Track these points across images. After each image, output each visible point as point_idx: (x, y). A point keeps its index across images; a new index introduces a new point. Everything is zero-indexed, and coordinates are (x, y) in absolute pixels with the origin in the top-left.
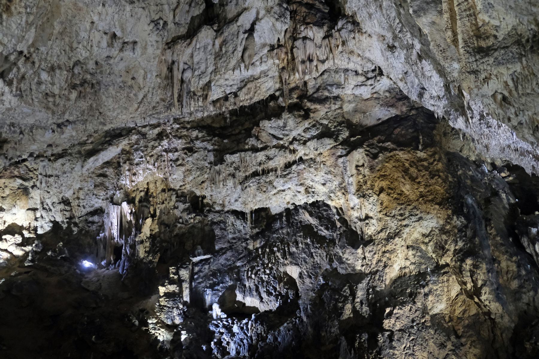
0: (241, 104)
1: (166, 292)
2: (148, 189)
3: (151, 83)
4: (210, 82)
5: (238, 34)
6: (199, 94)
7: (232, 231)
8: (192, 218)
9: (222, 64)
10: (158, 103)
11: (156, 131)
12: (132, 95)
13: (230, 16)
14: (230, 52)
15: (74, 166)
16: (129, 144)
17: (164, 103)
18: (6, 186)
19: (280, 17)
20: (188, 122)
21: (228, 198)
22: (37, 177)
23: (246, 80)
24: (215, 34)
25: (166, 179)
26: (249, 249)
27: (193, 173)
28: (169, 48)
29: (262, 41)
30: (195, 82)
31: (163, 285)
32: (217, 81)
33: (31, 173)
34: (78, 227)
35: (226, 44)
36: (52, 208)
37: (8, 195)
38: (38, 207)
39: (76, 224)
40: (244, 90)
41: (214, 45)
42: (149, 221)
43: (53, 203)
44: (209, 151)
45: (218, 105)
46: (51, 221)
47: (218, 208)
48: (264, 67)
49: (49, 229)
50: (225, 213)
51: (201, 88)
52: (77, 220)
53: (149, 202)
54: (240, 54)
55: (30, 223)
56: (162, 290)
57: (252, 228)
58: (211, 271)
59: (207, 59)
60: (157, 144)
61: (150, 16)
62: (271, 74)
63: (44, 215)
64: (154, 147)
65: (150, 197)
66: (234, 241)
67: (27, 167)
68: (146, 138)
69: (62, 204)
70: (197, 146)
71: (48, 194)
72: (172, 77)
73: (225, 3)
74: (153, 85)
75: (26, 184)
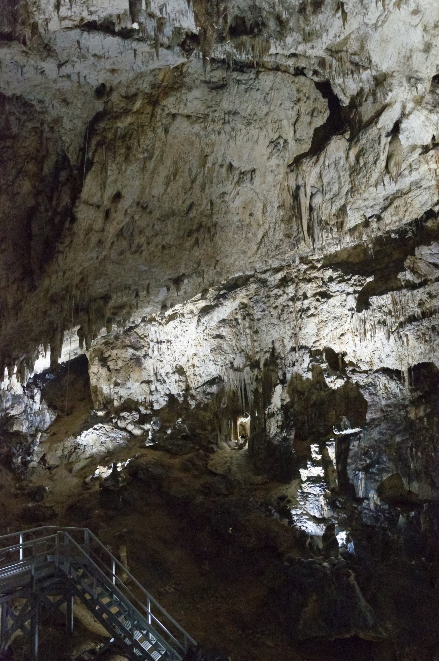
0: (388, 228)
1: (309, 476)
2: (273, 349)
3: (273, 217)
4: (344, 206)
5: (379, 138)
6: (332, 223)
7: (385, 395)
8: (332, 382)
9: (361, 181)
10: (281, 240)
11: (279, 276)
12: (250, 235)
13: (366, 118)
14: (371, 163)
15: (187, 328)
16: (247, 295)
17: (288, 240)
18: (119, 358)
19: (435, 107)
20: (318, 261)
21: (377, 353)
22: (149, 344)
23: (391, 197)
24: (348, 144)
25: (296, 334)
26: (410, 418)
27: (330, 324)
28: (292, 171)
29: (411, 142)
30: (327, 208)
31: (306, 468)
32: (353, 203)
33: (142, 341)
34: (196, 400)
35: (364, 154)
36: (166, 379)
37: (121, 368)
38: (153, 378)
39: (193, 397)
40: (391, 210)
41: (347, 158)
42: (279, 389)
43: (167, 373)
44: (348, 294)
45: (357, 233)
46: (167, 395)
47: (364, 367)
48: (415, 176)
49: (164, 403)
50: (374, 373)
51: (334, 215)
52: (193, 392)
53: (277, 365)
54: (384, 164)
55: (145, 398)
56: (304, 473)
57: (412, 391)
58: (362, 449)
59: (339, 178)
60: (281, 292)
61: (269, 136)
62: (425, 184)
63: (159, 387)
64: (277, 296)
65: (277, 359)
66: (388, 409)
67: (138, 334)
68: (267, 286)
69: (177, 374)
70: (331, 289)
71: (161, 364)
72: (299, 204)
73: (358, 103)
74: (274, 220)
75: (138, 353)
